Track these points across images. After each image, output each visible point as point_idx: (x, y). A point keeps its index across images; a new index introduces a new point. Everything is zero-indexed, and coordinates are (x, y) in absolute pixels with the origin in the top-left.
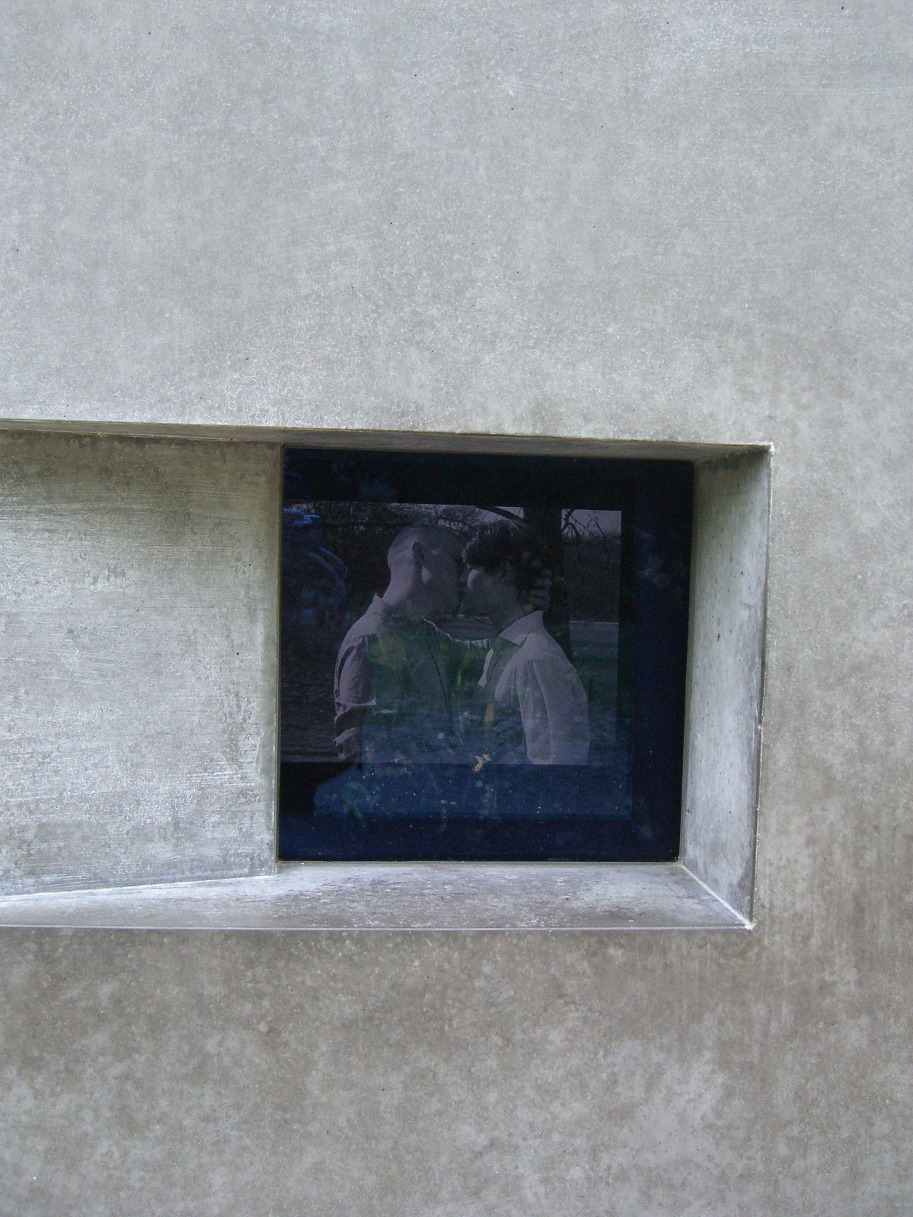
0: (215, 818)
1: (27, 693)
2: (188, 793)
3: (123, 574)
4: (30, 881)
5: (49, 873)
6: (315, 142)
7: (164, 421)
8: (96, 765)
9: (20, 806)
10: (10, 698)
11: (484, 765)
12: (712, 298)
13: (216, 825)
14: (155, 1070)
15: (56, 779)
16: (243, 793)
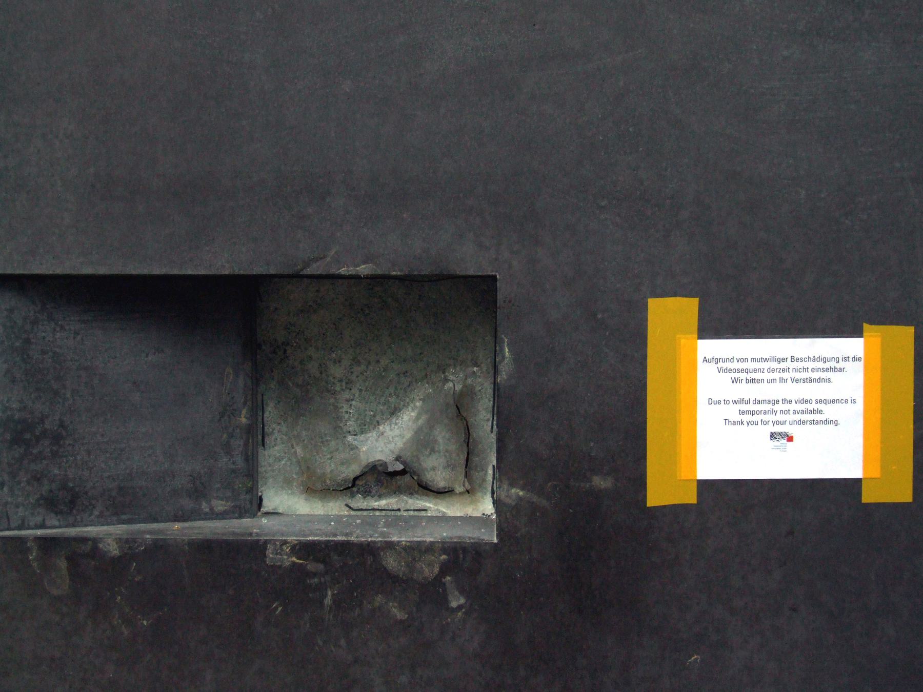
0: (218, 485)
1: (111, 416)
2: (202, 471)
3: (162, 351)
4: (115, 518)
5: (125, 514)
6: (244, 123)
7: (172, 273)
8: (149, 455)
9: (109, 477)
10: (102, 419)
11: (512, 485)
12: (461, 195)
13: (218, 489)
14: (64, 433)
15: (128, 463)
16: (234, 471)
